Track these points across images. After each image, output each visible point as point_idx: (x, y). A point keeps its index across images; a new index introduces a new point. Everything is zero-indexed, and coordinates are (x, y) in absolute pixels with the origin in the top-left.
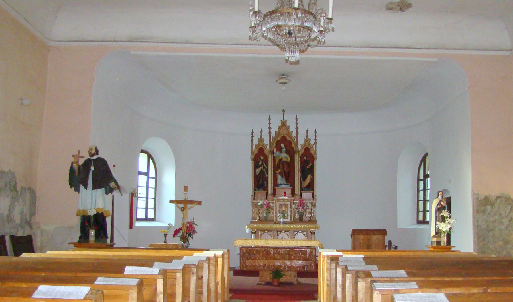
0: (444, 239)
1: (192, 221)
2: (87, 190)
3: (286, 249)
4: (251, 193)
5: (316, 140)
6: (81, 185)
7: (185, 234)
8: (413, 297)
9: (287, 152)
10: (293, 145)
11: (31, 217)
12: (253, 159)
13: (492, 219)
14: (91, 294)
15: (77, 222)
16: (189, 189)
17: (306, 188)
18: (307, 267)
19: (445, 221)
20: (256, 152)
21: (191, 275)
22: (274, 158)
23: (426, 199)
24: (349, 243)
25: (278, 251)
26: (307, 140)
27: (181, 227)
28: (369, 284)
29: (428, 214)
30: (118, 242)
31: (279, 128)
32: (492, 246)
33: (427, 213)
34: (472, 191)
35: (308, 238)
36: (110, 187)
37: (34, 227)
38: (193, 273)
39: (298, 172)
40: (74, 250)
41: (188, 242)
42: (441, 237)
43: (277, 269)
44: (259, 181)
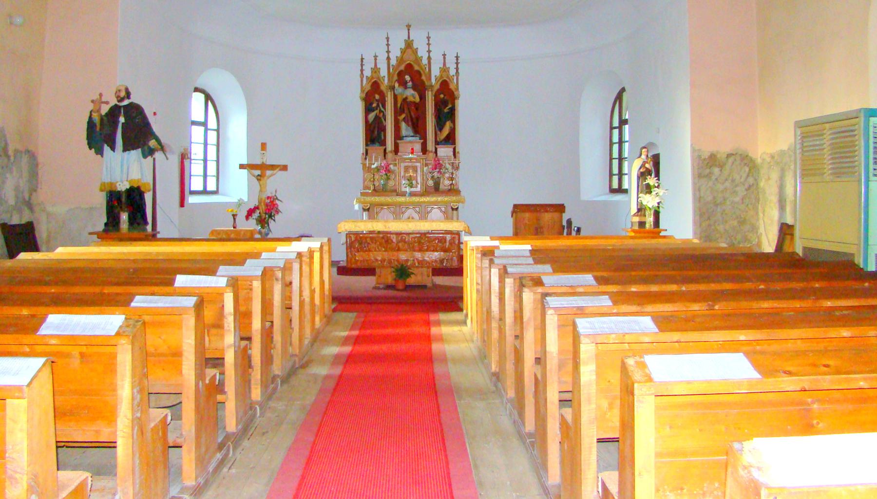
0: (650, 220)
1: (273, 195)
2: (114, 152)
3: (415, 235)
5: (457, 69)
7: (264, 215)
9: (414, 88)
10: (423, 78)
11: (31, 195)
12: (363, 99)
13: (720, 187)
14: (128, 326)
15: (100, 201)
17: (443, 142)
18: (447, 261)
19: (651, 192)
20: (368, 88)
21: (275, 282)
23: (623, 157)
24: (508, 225)
25: (404, 238)
26: (444, 69)
27: (257, 204)
28: (539, 296)
29: (625, 179)
30: (163, 230)
32: (721, 228)
33: (625, 128)
34: (692, 145)
35: (448, 218)
36: (150, 148)
37: (37, 209)
38: (277, 279)
39: (432, 118)
40: (97, 245)
41: (268, 225)
42: (645, 216)
44: (373, 132)
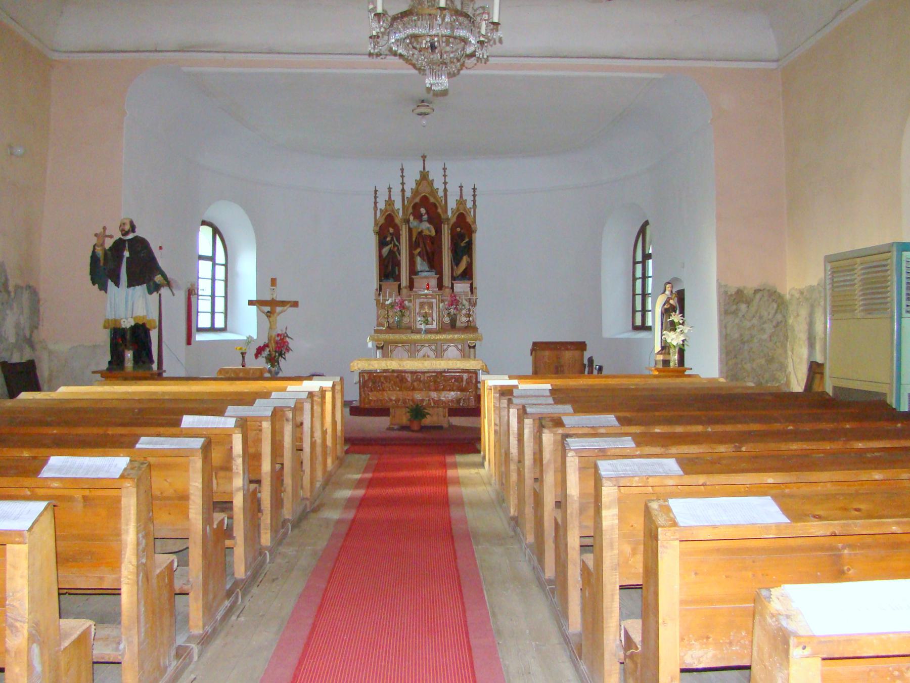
0: (674, 358)
2: (118, 287)
3: (431, 374)
5: (474, 201)
6: (110, 281)
7: (274, 353)
8: (627, 465)
9: (430, 221)
10: (439, 210)
11: (32, 332)
13: (747, 324)
14: (132, 469)
15: (104, 338)
16: (278, 281)
19: (676, 329)
20: (382, 221)
21: (285, 422)
22: (410, 230)
24: (527, 363)
26: (461, 202)
27: (267, 342)
28: (559, 438)
29: (649, 315)
30: (169, 369)
31: (416, 184)
32: (748, 367)
34: (718, 280)
35: (465, 356)
36: (155, 283)
38: (287, 420)
39: (448, 252)
40: (101, 384)
41: (278, 364)
42: (669, 354)
43: (417, 405)
44: (387, 267)
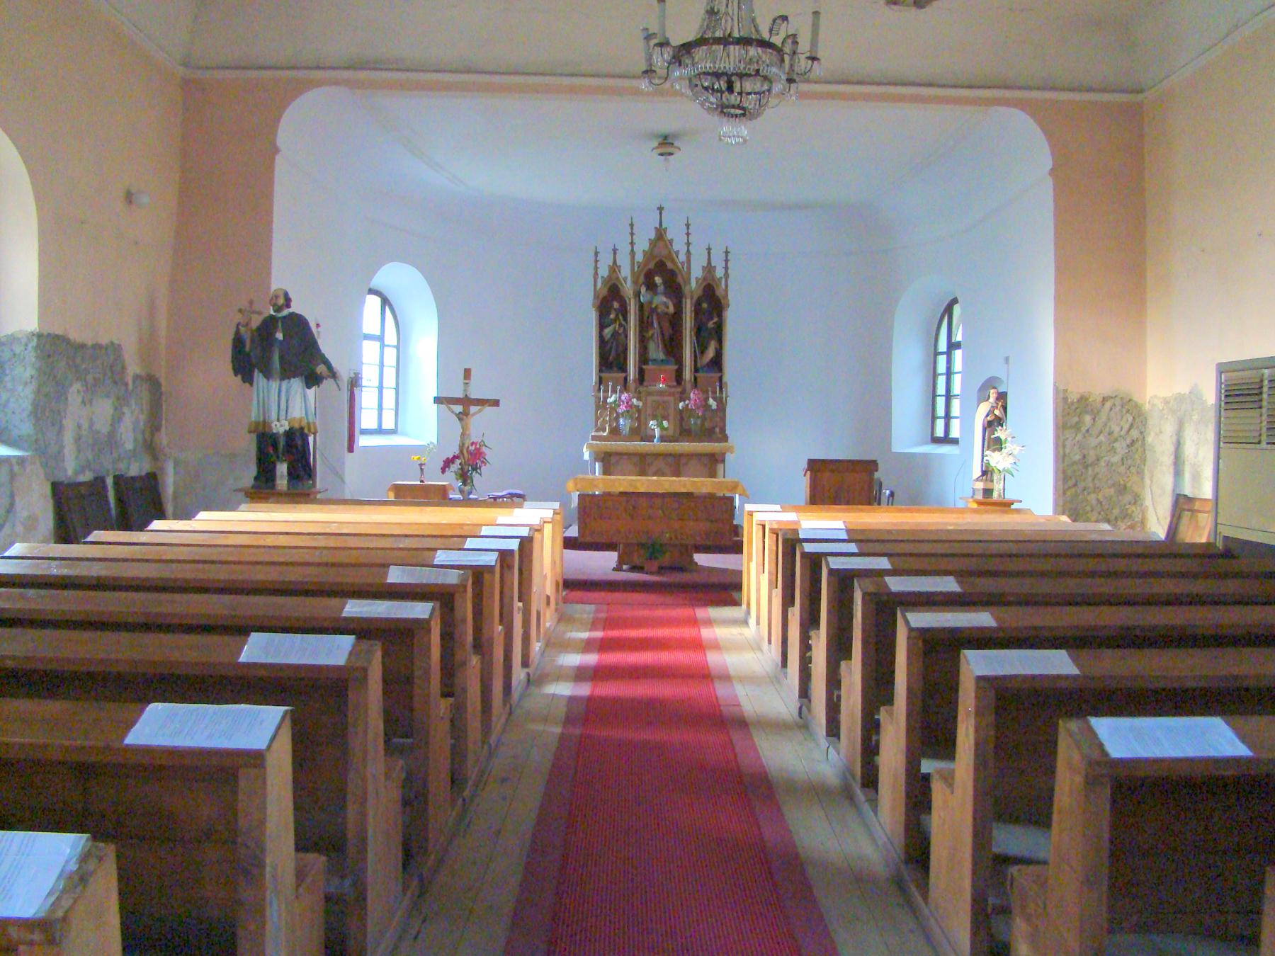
4: (594, 379)
5: (726, 268)
10: (680, 279)
13: (1093, 442)
15: (249, 446)
16: (473, 373)
20: (605, 292)
22: (641, 306)
24: (802, 484)
26: (709, 269)
31: (650, 244)
34: (1055, 383)
39: (691, 335)
42: (992, 481)
